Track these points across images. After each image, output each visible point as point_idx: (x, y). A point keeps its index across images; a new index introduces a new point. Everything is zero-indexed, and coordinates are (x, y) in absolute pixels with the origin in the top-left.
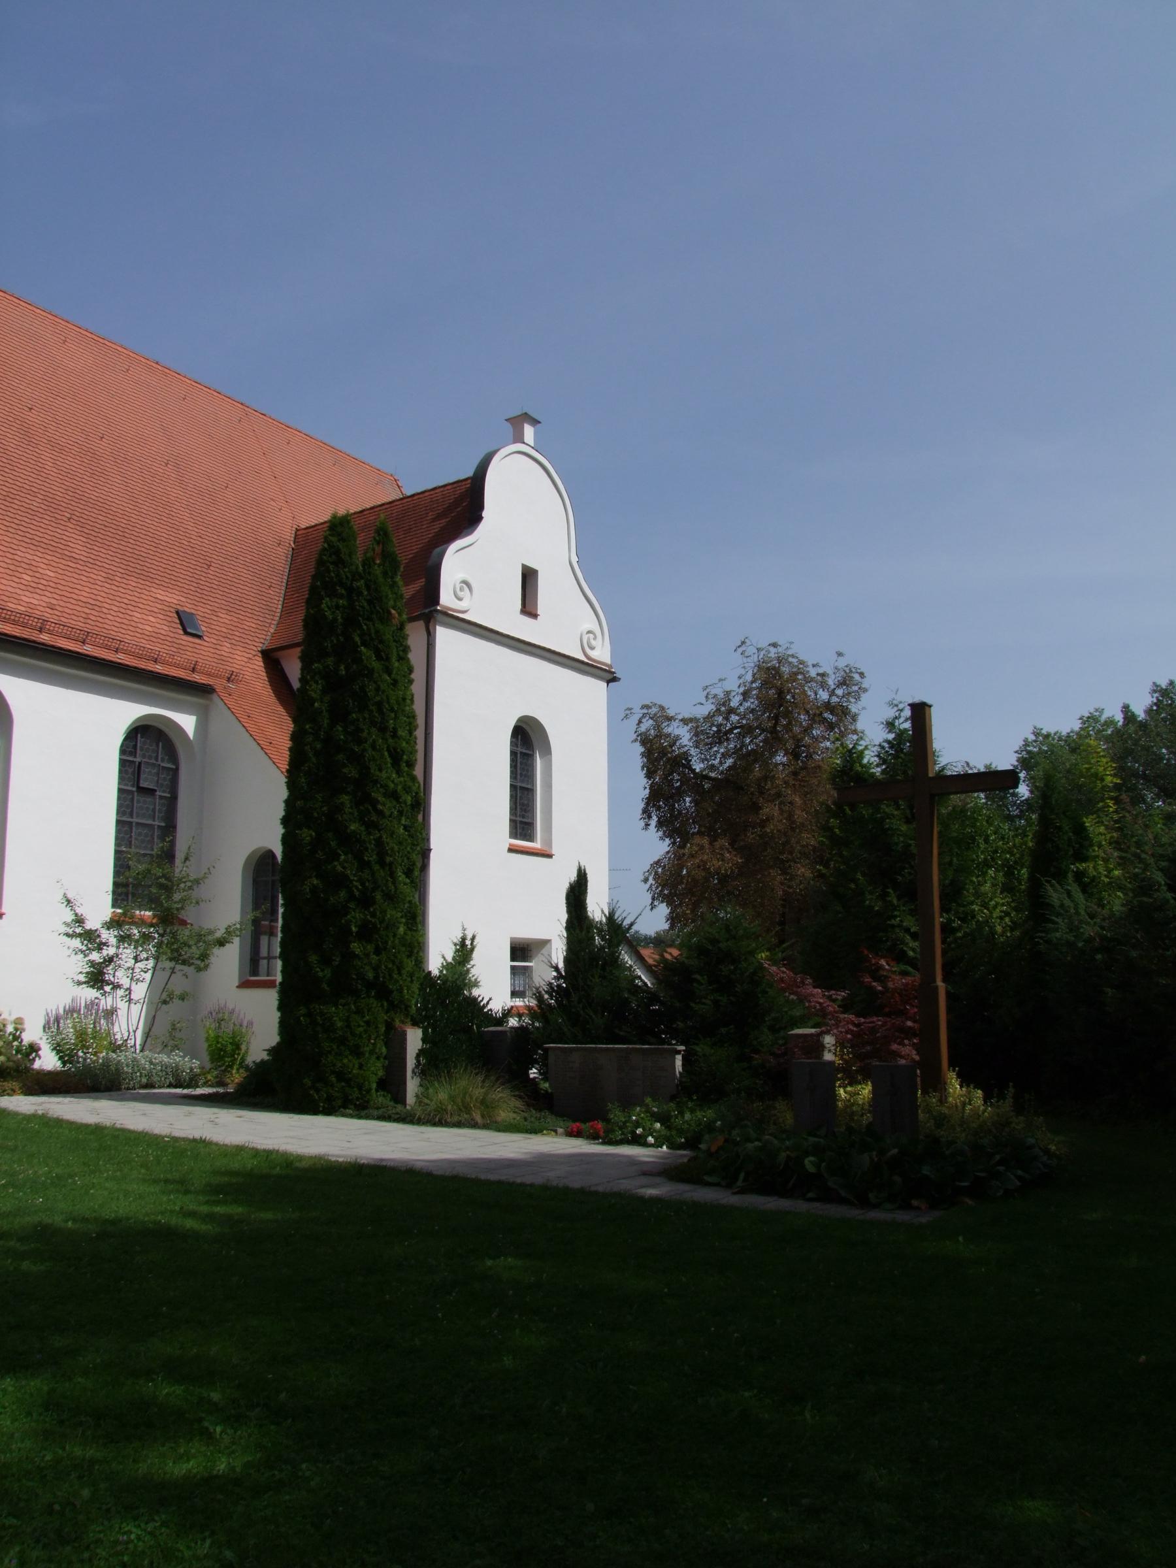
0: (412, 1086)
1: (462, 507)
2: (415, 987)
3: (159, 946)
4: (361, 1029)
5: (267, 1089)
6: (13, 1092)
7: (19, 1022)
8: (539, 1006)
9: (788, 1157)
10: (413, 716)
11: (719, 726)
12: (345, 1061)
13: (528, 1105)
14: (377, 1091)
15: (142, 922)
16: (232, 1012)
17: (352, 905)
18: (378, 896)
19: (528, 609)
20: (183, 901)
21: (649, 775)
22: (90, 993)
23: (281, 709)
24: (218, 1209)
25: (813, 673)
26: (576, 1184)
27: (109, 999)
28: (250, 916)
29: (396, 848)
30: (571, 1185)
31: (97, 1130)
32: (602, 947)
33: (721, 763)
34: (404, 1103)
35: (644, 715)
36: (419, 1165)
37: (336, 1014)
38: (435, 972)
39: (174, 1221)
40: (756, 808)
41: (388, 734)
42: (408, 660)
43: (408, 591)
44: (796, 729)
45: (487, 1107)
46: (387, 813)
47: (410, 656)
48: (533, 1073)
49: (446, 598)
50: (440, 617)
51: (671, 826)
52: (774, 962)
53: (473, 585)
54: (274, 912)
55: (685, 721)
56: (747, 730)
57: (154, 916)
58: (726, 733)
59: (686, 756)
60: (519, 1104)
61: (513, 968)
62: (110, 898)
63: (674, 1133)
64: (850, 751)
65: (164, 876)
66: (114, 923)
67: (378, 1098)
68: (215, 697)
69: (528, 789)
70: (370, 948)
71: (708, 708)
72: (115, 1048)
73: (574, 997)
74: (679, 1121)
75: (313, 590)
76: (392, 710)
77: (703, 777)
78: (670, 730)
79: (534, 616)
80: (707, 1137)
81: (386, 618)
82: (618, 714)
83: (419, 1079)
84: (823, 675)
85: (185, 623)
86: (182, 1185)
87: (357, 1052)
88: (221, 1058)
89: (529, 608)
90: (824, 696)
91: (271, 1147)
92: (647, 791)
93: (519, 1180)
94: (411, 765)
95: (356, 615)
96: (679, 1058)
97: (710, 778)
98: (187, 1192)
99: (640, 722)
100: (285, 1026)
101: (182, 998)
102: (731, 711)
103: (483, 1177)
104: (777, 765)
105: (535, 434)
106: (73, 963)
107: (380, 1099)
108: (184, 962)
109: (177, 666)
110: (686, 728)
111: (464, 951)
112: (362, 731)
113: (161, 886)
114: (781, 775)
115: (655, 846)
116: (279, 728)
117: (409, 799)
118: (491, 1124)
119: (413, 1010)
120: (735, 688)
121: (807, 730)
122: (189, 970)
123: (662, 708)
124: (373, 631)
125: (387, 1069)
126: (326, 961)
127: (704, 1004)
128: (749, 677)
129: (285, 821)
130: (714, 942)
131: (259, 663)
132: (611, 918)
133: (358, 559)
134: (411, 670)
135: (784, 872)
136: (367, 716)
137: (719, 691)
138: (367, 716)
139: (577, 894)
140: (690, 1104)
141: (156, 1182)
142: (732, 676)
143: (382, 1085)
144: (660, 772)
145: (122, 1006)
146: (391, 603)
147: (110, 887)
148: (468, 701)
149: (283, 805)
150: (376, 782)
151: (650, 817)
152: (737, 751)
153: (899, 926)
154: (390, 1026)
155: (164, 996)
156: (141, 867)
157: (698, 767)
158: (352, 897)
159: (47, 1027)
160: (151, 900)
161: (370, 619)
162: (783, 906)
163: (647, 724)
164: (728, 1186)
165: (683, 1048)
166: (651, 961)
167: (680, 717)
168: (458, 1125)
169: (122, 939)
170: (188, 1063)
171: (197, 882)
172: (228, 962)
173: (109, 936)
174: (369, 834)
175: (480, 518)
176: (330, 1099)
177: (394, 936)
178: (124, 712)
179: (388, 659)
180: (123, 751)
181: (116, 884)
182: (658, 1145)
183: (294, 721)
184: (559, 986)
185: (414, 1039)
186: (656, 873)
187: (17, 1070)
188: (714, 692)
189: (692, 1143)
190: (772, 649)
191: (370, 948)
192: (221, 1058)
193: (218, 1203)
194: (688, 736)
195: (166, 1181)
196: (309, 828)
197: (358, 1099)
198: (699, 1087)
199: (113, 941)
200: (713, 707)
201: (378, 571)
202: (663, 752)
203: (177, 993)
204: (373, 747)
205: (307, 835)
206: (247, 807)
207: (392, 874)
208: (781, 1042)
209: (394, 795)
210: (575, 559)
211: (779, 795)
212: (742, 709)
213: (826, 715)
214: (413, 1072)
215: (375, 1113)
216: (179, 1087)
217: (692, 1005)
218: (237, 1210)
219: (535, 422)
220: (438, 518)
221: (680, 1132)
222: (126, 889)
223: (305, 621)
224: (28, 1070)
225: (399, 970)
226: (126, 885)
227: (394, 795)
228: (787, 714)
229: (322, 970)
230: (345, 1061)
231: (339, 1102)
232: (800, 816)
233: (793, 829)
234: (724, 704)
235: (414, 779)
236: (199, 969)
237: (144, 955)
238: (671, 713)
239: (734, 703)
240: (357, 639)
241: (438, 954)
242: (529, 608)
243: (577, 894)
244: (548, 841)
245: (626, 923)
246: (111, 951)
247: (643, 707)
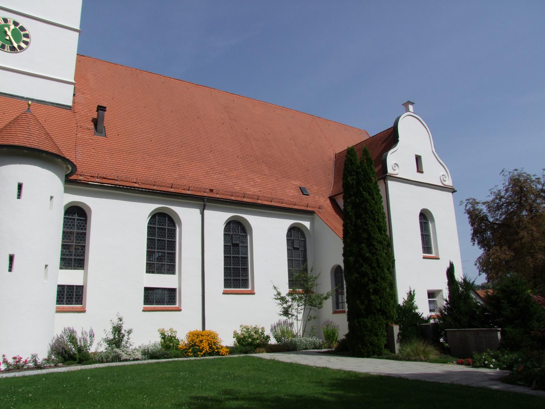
0: (397, 346)
1: (391, 138)
2: (395, 310)
3: (305, 301)
5: (345, 349)
6: (263, 352)
7: (263, 328)
8: (441, 315)
10: (384, 214)
11: (497, 203)
13: (441, 352)
15: (299, 293)
16: (331, 322)
17: (370, 282)
18: (379, 279)
19: (420, 170)
20: (312, 285)
22: (284, 318)
23: (338, 216)
24: (334, 392)
25: (534, 178)
26: (464, 383)
27: (291, 320)
28: (335, 288)
30: (462, 384)
31: (291, 364)
32: (463, 292)
33: (500, 217)
34: (395, 353)
35: (467, 203)
36: (403, 376)
37: (368, 321)
38: (401, 304)
39: (320, 396)
40: (517, 233)
42: (380, 194)
43: (376, 170)
44: (530, 201)
46: (379, 249)
47: (380, 193)
48: (442, 340)
49: (390, 171)
50: (388, 177)
51: (483, 243)
52: (535, 294)
54: (342, 286)
55: (484, 203)
56: (509, 204)
57: (303, 291)
58: (501, 206)
60: (437, 352)
61: (429, 301)
62: (288, 286)
63: (501, 363)
65: (305, 277)
66: (290, 294)
67: (384, 351)
68: (315, 214)
70: (378, 297)
71: (492, 197)
72: (294, 336)
73: (454, 311)
74: (502, 358)
75: (344, 174)
76: (376, 212)
77: (493, 223)
79: (422, 172)
80: (516, 365)
81: (370, 180)
82: (458, 204)
84: (538, 179)
85: (303, 191)
86: (321, 383)
87: (376, 335)
88: (329, 338)
89: (420, 170)
91: (349, 370)
92: (472, 231)
93: (441, 382)
94: (385, 231)
95: (360, 182)
98: (323, 386)
99: (466, 206)
100: (350, 327)
101: (314, 318)
102: (502, 197)
103: (427, 380)
104: (523, 216)
105: (413, 108)
106: (277, 308)
107: (386, 352)
108: (314, 306)
109: (302, 206)
110: (484, 206)
111: (411, 296)
113: (304, 280)
114: (526, 219)
115: (478, 251)
116: (338, 223)
118: (427, 360)
119: (395, 319)
121: (534, 201)
122: (316, 308)
123: (474, 199)
128: (507, 184)
129: (344, 255)
130: (508, 287)
131: (328, 201)
132: (465, 280)
133: (358, 162)
134: (381, 198)
135: (533, 257)
137: (495, 190)
139: (450, 272)
140: (506, 352)
141: (312, 382)
142: (501, 184)
143: (386, 346)
144: (476, 224)
145: (295, 322)
146: (371, 175)
147: (287, 282)
148: (402, 206)
149: (342, 250)
150: (373, 238)
151: (474, 241)
152: (506, 212)
154: (387, 325)
155: (308, 318)
156: (297, 275)
157: (491, 220)
159: (271, 330)
160: (301, 285)
161: (365, 182)
162: (534, 271)
163: (469, 206)
164: (529, 386)
165: (500, 329)
166: (482, 296)
168: (416, 360)
169: (293, 299)
170: (319, 341)
171: (316, 278)
172: (328, 304)
173: (289, 298)
175: (398, 141)
178: (285, 223)
179: (373, 195)
180: (288, 236)
181: (289, 281)
182: (495, 368)
183: (343, 220)
184: (448, 307)
185: (396, 329)
186: (480, 262)
187: (264, 344)
188: (494, 191)
189: (510, 367)
190: (515, 172)
191: (378, 297)
192: (329, 338)
193: (332, 390)
194: (486, 209)
195: (316, 382)
198: (508, 344)
199: (290, 300)
200: (494, 197)
201: (365, 165)
202: (477, 216)
203: (313, 316)
204: (371, 226)
205: (352, 259)
206: (330, 251)
207: (383, 270)
209: (381, 242)
210: (434, 150)
212: (506, 196)
213: (542, 194)
215: (385, 357)
216: (316, 349)
218: (340, 392)
219: (412, 104)
220: (383, 143)
221: (504, 363)
222: (292, 283)
223: (343, 185)
224: (267, 344)
225: (389, 304)
226: (293, 281)
227: (381, 242)
228: (525, 196)
231: (372, 353)
232: (536, 235)
233: (533, 240)
234: (498, 195)
235: (387, 236)
236: (319, 308)
237: (301, 304)
238: (478, 201)
239: (502, 194)
241: (401, 298)
242: (420, 170)
243: (450, 272)
244: (437, 253)
245: (471, 282)
246: (290, 303)
247: (467, 200)
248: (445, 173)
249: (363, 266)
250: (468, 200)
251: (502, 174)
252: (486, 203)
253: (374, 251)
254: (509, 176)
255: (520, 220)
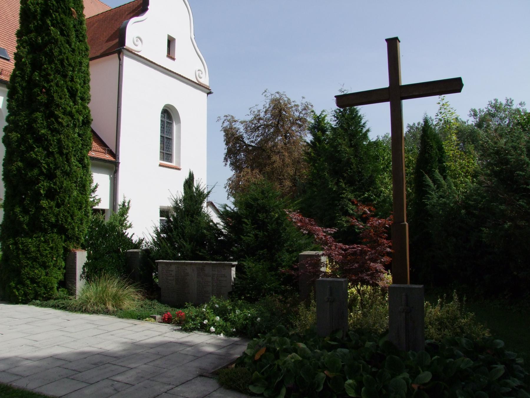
0: (80, 284)
4: (47, 252)
9: (328, 378)
12: (36, 271)
14: (58, 288)
17: (41, 178)
18: (58, 172)
19: (170, 56)
21: (227, 144)
29: (70, 145)
35: (225, 120)
37: (31, 243)
40: (269, 157)
41: (67, 79)
45: (117, 299)
46: (65, 124)
49: (129, 44)
51: (236, 166)
53: (142, 38)
55: (242, 123)
56: (267, 126)
59: (241, 137)
60: (140, 296)
61: (161, 220)
64: (318, 117)
69: (170, 139)
76: (70, 65)
78: (236, 126)
79: (174, 59)
83: (85, 281)
90: (297, 114)
92: (226, 151)
96: (234, 270)
97: (251, 146)
99: (224, 122)
112: (50, 75)
114: (280, 145)
115: (229, 173)
117: (81, 118)
119: (82, 240)
120: (262, 108)
123: (233, 117)
124: (59, 18)
125: (65, 275)
126: (25, 211)
127: (249, 236)
128: (268, 106)
130: (256, 200)
136: (53, 66)
138: (53, 66)
150: (58, 106)
151: (227, 161)
153: (346, 198)
154: (66, 250)
157: (247, 142)
158: (41, 173)
161: (57, 12)
167: (240, 121)
174: (54, 136)
176: (26, 294)
177: (69, 197)
179: (68, 36)
185: (81, 257)
194: (243, 128)
196: (17, 132)
197: (44, 293)
202: (233, 135)
204: (57, 85)
205: (14, 136)
207: (68, 160)
208: (294, 259)
209: (71, 114)
210: (193, 37)
211: (279, 152)
214: (81, 276)
217: (242, 237)
221: (233, 323)
225: (72, 216)
227: (71, 114)
228: (283, 120)
229: (23, 217)
230: (36, 271)
232: (288, 160)
238: (236, 119)
240: (49, 22)
244: (179, 163)
248: (202, 68)
249: (32, 149)
250: (226, 116)
251: (264, 94)
252: (244, 122)
253: (56, 126)
254: (270, 98)
255: (275, 145)
